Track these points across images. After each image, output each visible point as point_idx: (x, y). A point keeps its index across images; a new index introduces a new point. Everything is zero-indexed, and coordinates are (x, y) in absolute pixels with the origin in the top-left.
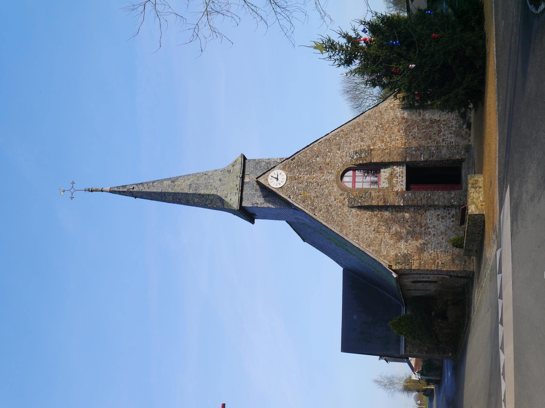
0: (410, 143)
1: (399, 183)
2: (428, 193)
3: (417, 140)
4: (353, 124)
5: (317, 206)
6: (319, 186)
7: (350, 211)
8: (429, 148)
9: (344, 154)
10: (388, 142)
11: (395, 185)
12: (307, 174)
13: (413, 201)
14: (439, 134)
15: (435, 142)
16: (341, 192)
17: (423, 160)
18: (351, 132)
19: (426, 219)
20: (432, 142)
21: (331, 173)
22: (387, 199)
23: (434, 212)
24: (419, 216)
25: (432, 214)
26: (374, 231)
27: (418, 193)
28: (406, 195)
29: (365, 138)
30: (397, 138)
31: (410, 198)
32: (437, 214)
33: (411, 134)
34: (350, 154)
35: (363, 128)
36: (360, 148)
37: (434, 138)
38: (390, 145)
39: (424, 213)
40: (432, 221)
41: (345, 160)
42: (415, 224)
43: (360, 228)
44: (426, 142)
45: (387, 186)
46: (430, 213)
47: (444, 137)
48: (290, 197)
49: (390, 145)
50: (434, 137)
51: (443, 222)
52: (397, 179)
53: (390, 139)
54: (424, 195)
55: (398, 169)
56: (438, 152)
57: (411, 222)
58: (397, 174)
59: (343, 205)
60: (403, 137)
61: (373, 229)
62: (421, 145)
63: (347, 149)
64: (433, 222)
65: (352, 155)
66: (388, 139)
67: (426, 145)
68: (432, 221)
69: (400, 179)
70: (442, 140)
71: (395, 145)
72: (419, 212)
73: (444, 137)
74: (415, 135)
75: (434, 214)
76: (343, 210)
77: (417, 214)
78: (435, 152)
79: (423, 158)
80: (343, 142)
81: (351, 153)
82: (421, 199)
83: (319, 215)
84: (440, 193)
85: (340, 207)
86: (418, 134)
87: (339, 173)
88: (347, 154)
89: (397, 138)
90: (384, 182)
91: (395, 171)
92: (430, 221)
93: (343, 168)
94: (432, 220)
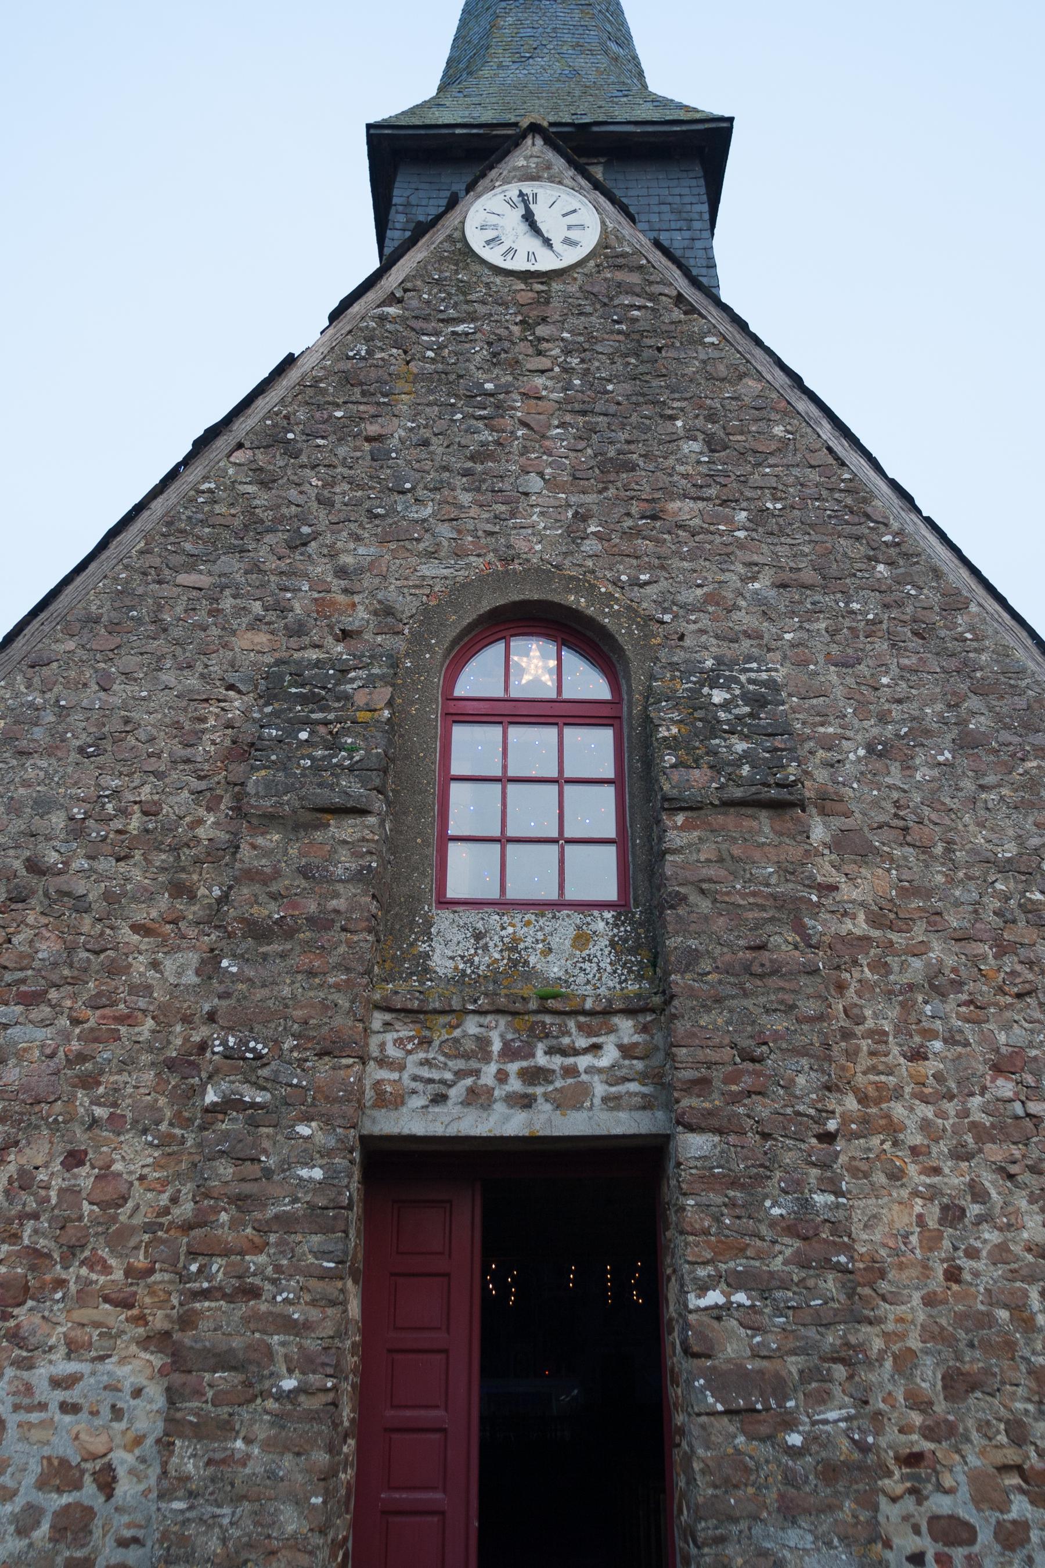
0: (896, 1176)
1: (460, 1074)
2: (305, 1364)
3: (931, 1242)
4: (1021, 672)
5: (304, 459)
6: (470, 464)
7: (232, 678)
8: (840, 1371)
9: (745, 619)
10: (881, 966)
11: (440, 1036)
12: (565, 389)
13: (241, 1201)
14: (1015, 1480)
15: (929, 1433)
16: (407, 605)
17: (694, 1301)
18: (953, 664)
19: (73, 1348)
20: (919, 1403)
21: (574, 534)
22: (283, 956)
23: (142, 1425)
24: (118, 1275)
25: (117, 1413)
26: (34, 867)
27: (316, 1255)
28: (304, 1130)
29: (908, 767)
30: (937, 1045)
31: (268, 1173)
32: (123, 1460)
33: (988, 1180)
34: (749, 659)
35: (996, 752)
36: (809, 738)
37: (970, 1423)
38: (854, 986)
39: (141, 1319)
40: (54, 1407)
41: (684, 627)
42: (36, 1231)
43: (74, 756)
44: (914, 1342)
45: (442, 962)
46: (137, 1393)
47: (985, 1536)
48: (392, 299)
49: (854, 986)
50: (984, 1427)
51: (22, 1532)
52: (497, 1046)
53: (911, 987)
54: (288, 1325)
55: (604, 1062)
56: (790, 1479)
57: (70, 1193)
58: (550, 1052)
59: (298, 630)
60: (951, 1107)
61: (53, 857)
62: (883, 1286)
63: (788, 636)
64: (35, 1417)
65: (743, 678)
66: (917, 963)
67: (878, 1344)
68: (42, 1406)
69: (502, 1077)
70: (952, 1518)
71: (859, 1030)
72: (157, 1277)
73: (985, 1536)
74: (980, 1220)
75: (119, 1426)
76: (251, 627)
77: (140, 1261)
78: (795, 1439)
79: (717, 1313)
80: (855, 606)
81: (754, 665)
82: (254, 1293)
83: (231, 471)
84: (300, 1502)
85: (282, 609)
86: (1001, 1254)
87: (577, 591)
88: (746, 643)
89: (937, 1045)
90: (478, 936)
91: (586, 1030)
92: (56, 1383)
93: (612, 615)
94: (67, 1408)
